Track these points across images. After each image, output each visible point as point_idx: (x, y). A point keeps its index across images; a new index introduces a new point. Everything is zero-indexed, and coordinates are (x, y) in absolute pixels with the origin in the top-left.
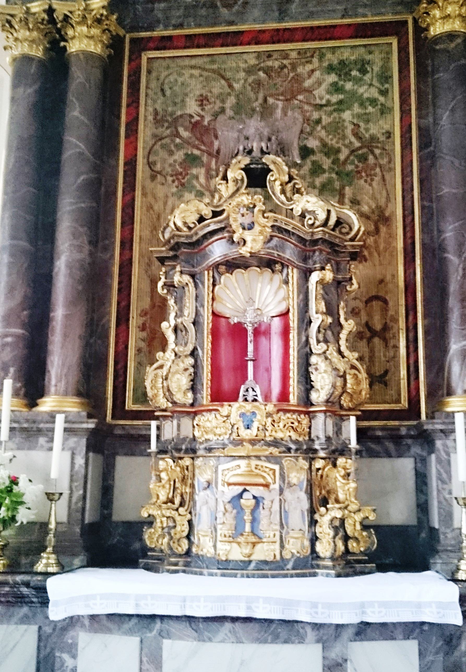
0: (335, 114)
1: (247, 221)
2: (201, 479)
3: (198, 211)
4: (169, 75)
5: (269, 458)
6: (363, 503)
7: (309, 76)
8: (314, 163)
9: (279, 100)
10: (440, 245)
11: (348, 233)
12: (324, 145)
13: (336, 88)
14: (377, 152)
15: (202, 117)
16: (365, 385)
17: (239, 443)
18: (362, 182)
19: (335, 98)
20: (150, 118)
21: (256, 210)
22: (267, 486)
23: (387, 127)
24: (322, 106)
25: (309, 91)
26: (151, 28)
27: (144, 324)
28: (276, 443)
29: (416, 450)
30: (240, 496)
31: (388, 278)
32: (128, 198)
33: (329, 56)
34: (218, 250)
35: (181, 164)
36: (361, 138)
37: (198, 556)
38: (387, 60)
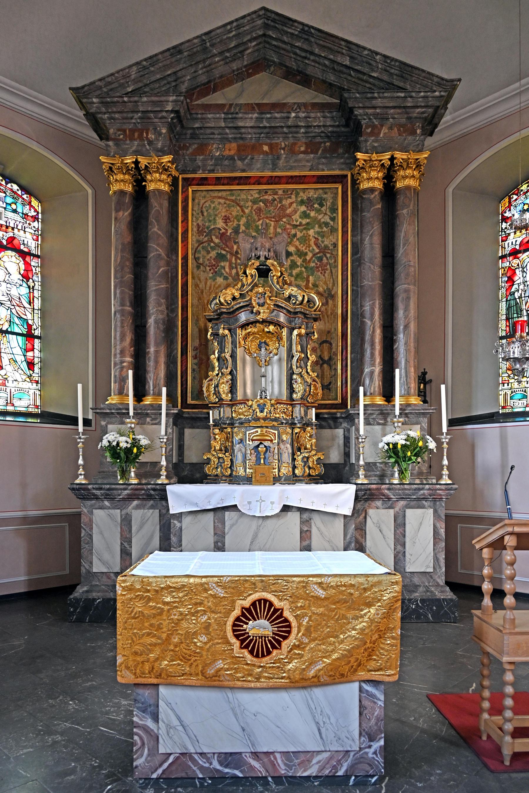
0: (305, 232)
1: (262, 301)
2: (237, 438)
3: (233, 294)
4: (205, 202)
5: (273, 427)
6: (318, 451)
7: (290, 207)
8: (292, 261)
9: (271, 221)
10: (361, 314)
11: (313, 307)
12: (298, 250)
13: (305, 215)
14: (328, 255)
15: (227, 230)
16: (320, 391)
17: (258, 419)
18: (319, 273)
19: (304, 222)
20: (195, 229)
21: (266, 295)
22: (271, 441)
23: (334, 240)
24: (297, 226)
25: (289, 216)
26: (194, 172)
27: (196, 355)
28: (276, 419)
29: (345, 425)
30: (258, 446)
31: (333, 330)
32: (184, 280)
33: (301, 194)
34: (243, 317)
35: (214, 259)
36: (319, 247)
37: (236, 476)
38: (335, 198)
